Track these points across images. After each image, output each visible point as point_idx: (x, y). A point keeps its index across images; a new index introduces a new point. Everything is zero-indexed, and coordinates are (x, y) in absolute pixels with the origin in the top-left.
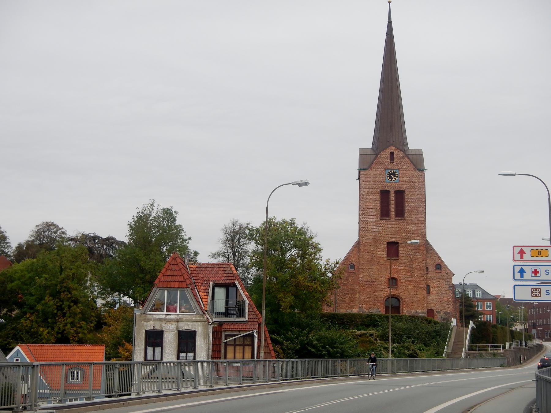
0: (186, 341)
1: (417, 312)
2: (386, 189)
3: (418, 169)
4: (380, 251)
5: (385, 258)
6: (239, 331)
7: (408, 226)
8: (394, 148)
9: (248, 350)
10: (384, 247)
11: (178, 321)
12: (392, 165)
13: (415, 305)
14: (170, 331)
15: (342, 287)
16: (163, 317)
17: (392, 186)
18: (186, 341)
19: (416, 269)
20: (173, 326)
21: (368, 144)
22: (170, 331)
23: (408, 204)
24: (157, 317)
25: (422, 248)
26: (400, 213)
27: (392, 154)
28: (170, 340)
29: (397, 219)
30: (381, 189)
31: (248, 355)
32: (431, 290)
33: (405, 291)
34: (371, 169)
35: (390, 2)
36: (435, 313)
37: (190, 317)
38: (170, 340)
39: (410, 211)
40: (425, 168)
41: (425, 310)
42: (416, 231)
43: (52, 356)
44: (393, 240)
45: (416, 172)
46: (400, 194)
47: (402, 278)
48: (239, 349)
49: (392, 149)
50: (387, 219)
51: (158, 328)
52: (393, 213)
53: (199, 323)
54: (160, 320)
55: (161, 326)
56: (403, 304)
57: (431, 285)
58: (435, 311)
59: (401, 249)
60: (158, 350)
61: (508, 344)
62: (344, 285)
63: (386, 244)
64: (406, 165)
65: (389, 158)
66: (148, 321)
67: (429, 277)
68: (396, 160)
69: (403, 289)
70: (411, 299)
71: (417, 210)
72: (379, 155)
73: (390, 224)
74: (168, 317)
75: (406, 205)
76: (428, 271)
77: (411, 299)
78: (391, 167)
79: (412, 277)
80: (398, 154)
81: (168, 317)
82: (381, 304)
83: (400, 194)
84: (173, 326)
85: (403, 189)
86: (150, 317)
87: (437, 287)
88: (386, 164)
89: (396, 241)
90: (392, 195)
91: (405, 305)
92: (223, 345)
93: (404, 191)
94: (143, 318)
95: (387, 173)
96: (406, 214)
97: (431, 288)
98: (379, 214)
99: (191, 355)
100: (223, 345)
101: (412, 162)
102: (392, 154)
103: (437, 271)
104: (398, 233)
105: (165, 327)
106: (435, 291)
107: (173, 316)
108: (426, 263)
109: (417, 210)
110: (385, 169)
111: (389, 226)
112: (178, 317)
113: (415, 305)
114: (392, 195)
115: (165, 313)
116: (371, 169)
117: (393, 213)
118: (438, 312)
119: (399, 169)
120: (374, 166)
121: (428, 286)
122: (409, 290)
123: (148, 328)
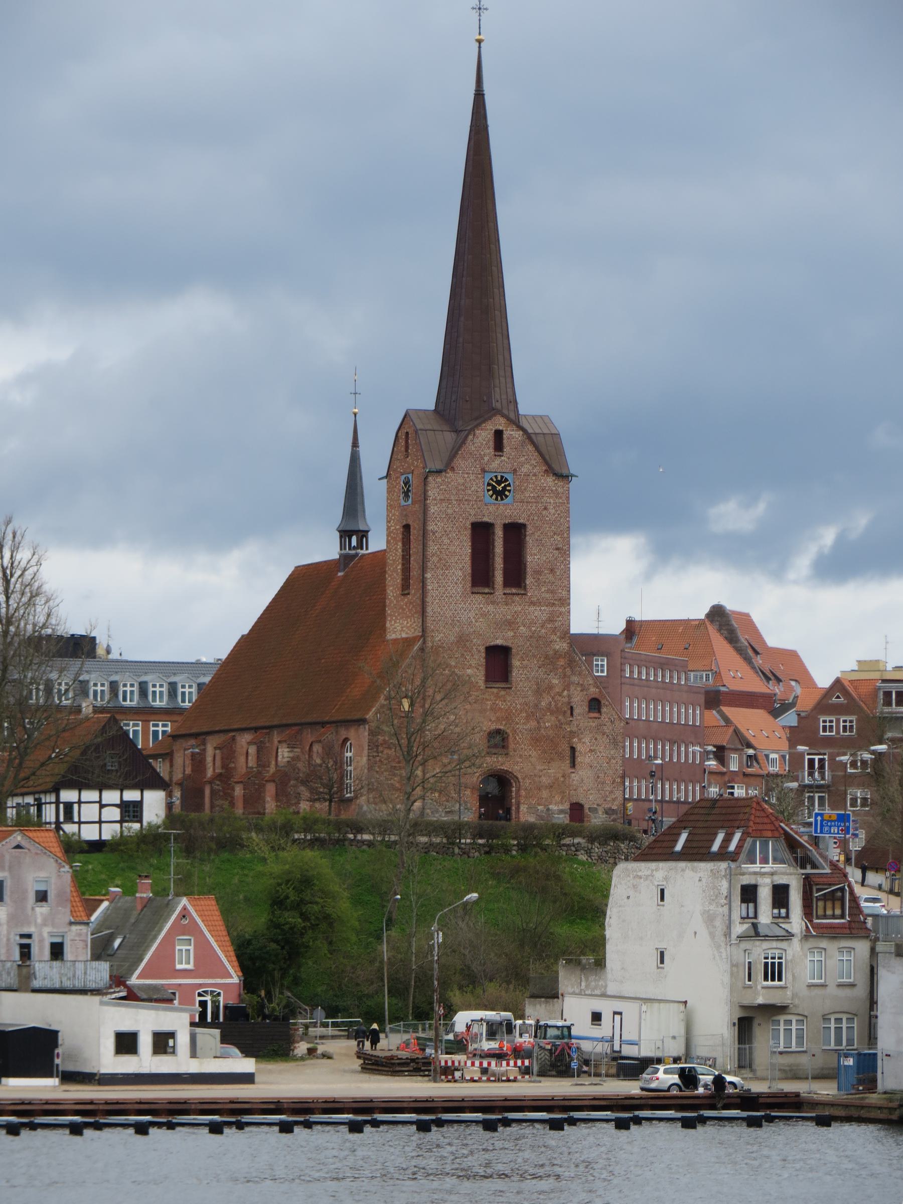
0: (780, 895)
1: (548, 810)
2: (486, 519)
3: (555, 474)
4: (470, 667)
5: (481, 684)
7: (532, 608)
8: (502, 420)
9: (838, 904)
11: (772, 874)
13: (545, 794)
14: (765, 885)
15: (386, 751)
16: (758, 870)
17: (498, 513)
18: (780, 895)
20: (768, 880)
21: (425, 397)
22: (765, 885)
23: (534, 557)
24: (752, 870)
25: (562, 662)
26: (516, 577)
27: (498, 434)
28: (765, 895)
29: (508, 591)
30: (473, 519)
31: (838, 912)
32: (579, 759)
33: (523, 762)
34: (453, 469)
35: (479, 42)
36: (587, 811)
37: (784, 870)
38: (765, 895)
39: (538, 572)
40: (572, 471)
41: (566, 806)
42: (551, 620)
44: (499, 642)
45: (550, 480)
47: (521, 730)
48: (829, 904)
49: (499, 423)
50: (487, 590)
51: (753, 882)
52: (499, 577)
53: (793, 877)
54: (755, 873)
55: (756, 880)
56: (518, 791)
57: (579, 747)
58: (586, 806)
59: (516, 663)
60: (751, 905)
61: (587, 740)
63: (482, 649)
65: (492, 444)
66: (743, 874)
69: (521, 756)
70: (537, 779)
72: (471, 437)
73: (493, 603)
74: (763, 870)
75: (529, 558)
76: (572, 714)
77: (537, 779)
79: (539, 728)
80: (512, 435)
82: (472, 793)
84: (768, 880)
85: (521, 521)
86: (745, 871)
87: (591, 751)
88: (486, 459)
89: (505, 644)
90: (499, 533)
91: (523, 793)
92: (815, 899)
93: (524, 526)
94: (738, 871)
95: (487, 480)
97: (577, 754)
98: (469, 578)
99: (783, 911)
100: (815, 899)
101: (541, 454)
102: (498, 434)
103: (592, 715)
104: (510, 624)
106: (587, 760)
107: (767, 868)
108: (569, 696)
110: (484, 471)
111: (491, 608)
112: (772, 870)
113: (545, 794)
114: (499, 533)
115: (770, 865)
116: (453, 469)
117: (499, 577)
119: (515, 471)
120: (458, 462)
121: (573, 749)
122: (533, 760)
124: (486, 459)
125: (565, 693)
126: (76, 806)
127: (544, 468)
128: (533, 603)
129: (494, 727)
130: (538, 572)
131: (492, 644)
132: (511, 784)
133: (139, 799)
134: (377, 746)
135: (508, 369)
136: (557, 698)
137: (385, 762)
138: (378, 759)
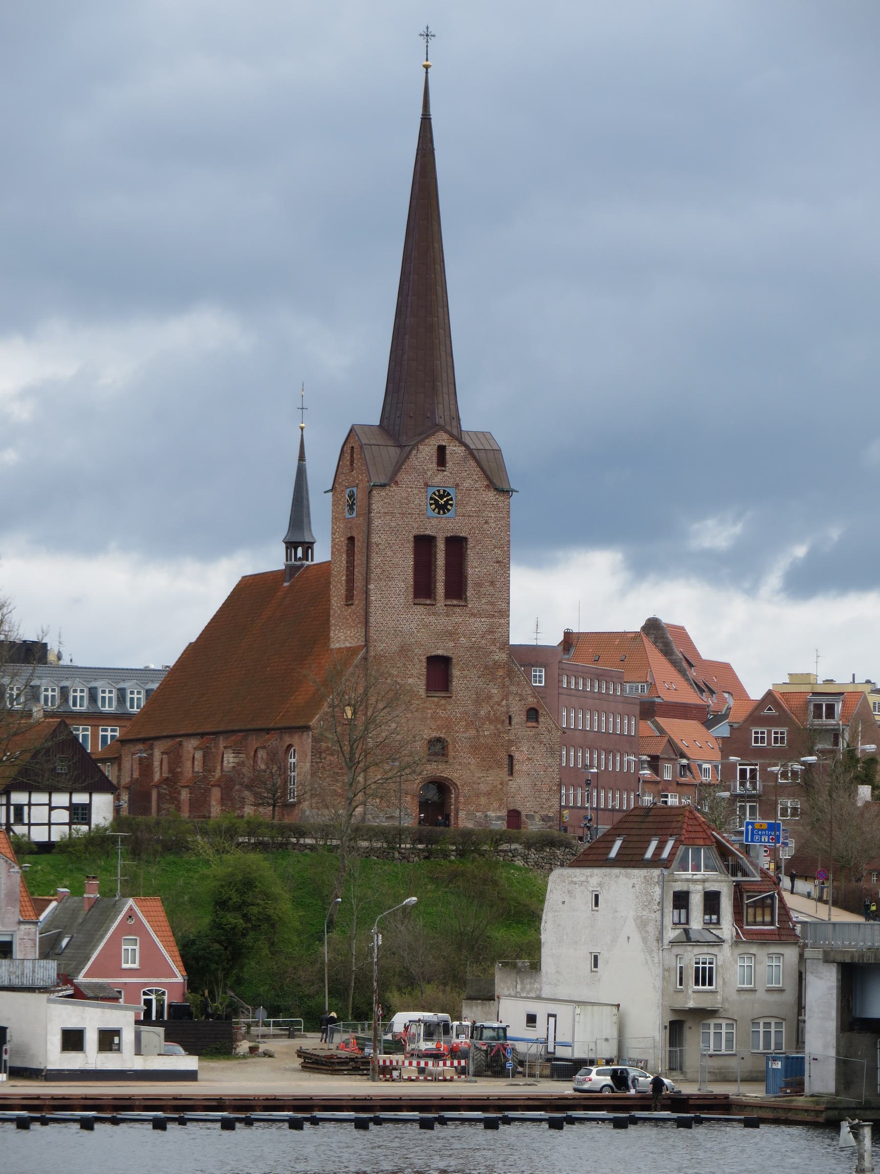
0: (712, 901)
1: (486, 816)
2: (428, 532)
3: (496, 489)
4: (412, 676)
5: (422, 693)
6: (760, 892)
7: (473, 620)
8: (445, 436)
9: (768, 911)
10: (420, 668)
12: (440, 476)
13: (483, 800)
14: (697, 892)
16: (690, 877)
17: (441, 527)
18: (712, 901)
19: (487, 718)
20: (699, 887)
23: (474, 569)
24: (684, 877)
25: (501, 673)
26: (457, 589)
27: (441, 450)
28: (696, 902)
30: (416, 532)
31: (768, 919)
32: (516, 767)
33: (462, 770)
34: (396, 483)
35: (427, 67)
37: (715, 877)
38: (696, 902)
39: (479, 585)
41: (504, 813)
43: (155, 914)
44: (440, 652)
45: (491, 496)
46: (457, 545)
48: (759, 911)
49: (442, 438)
50: (428, 602)
51: (685, 889)
53: (724, 884)
54: (687, 880)
56: (457, 797)
57: (517, 756)
58: (523, 813)
59: (456, 672)
60: (683, 911)
62: (332, 755)
63: (424, 659)
64: (460, 476)
65: (435, 459)
66: (676, 881)
67: (513, 738)
68: (449, 465)
69: (460, 764)
70: (475, 786)
71: (492, 583)
72: (414, 452)
73: (434, 614)
74: (695, 877)
75: (470, 571)
76: (510, 723)
78: (440, 480)
79: (478, 737)
80: (454, 450)
81: (695, 877)
83: (457, 545)
84: (699, 887)
85: (463, 535)
86: (678, 877)
87: (529, 759)
88: (429, 473)
89: (445, 654)
90: (441, 546)
93: (465, 539)
95: (430, 494)
96: (470, 593)
97: (515, 762)
98: (411, 590)
99: (714, 917)
102: (441, 450)
103: (530, 724)
104: (451, 635)
105: (693, 887)
107: (700, 875)
109: (492, 583)
110: (427, 485)
111: (432, 619)
113: (483, 800)
114: (441, 546)
116: (396, 483)
118: (530, 817)
119: (457, 485)
120: (402, 477)
121: (511, 758)
122: (472, 767)
123: (677, 889)
124: (429, 473)
125: (504, 702)
126: (26, 808)
127: (486, 483)
128: (473, 615)
129: (435, 734)
130: (479, 585)
131: (433, 654)
132: (450, 791)
133: (88, 802)
134: (321, 753)
135: (452, 386)
136: (496, 707)
137: (328, 768)
138: (321, 765)
